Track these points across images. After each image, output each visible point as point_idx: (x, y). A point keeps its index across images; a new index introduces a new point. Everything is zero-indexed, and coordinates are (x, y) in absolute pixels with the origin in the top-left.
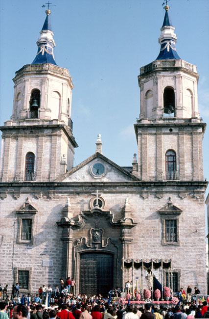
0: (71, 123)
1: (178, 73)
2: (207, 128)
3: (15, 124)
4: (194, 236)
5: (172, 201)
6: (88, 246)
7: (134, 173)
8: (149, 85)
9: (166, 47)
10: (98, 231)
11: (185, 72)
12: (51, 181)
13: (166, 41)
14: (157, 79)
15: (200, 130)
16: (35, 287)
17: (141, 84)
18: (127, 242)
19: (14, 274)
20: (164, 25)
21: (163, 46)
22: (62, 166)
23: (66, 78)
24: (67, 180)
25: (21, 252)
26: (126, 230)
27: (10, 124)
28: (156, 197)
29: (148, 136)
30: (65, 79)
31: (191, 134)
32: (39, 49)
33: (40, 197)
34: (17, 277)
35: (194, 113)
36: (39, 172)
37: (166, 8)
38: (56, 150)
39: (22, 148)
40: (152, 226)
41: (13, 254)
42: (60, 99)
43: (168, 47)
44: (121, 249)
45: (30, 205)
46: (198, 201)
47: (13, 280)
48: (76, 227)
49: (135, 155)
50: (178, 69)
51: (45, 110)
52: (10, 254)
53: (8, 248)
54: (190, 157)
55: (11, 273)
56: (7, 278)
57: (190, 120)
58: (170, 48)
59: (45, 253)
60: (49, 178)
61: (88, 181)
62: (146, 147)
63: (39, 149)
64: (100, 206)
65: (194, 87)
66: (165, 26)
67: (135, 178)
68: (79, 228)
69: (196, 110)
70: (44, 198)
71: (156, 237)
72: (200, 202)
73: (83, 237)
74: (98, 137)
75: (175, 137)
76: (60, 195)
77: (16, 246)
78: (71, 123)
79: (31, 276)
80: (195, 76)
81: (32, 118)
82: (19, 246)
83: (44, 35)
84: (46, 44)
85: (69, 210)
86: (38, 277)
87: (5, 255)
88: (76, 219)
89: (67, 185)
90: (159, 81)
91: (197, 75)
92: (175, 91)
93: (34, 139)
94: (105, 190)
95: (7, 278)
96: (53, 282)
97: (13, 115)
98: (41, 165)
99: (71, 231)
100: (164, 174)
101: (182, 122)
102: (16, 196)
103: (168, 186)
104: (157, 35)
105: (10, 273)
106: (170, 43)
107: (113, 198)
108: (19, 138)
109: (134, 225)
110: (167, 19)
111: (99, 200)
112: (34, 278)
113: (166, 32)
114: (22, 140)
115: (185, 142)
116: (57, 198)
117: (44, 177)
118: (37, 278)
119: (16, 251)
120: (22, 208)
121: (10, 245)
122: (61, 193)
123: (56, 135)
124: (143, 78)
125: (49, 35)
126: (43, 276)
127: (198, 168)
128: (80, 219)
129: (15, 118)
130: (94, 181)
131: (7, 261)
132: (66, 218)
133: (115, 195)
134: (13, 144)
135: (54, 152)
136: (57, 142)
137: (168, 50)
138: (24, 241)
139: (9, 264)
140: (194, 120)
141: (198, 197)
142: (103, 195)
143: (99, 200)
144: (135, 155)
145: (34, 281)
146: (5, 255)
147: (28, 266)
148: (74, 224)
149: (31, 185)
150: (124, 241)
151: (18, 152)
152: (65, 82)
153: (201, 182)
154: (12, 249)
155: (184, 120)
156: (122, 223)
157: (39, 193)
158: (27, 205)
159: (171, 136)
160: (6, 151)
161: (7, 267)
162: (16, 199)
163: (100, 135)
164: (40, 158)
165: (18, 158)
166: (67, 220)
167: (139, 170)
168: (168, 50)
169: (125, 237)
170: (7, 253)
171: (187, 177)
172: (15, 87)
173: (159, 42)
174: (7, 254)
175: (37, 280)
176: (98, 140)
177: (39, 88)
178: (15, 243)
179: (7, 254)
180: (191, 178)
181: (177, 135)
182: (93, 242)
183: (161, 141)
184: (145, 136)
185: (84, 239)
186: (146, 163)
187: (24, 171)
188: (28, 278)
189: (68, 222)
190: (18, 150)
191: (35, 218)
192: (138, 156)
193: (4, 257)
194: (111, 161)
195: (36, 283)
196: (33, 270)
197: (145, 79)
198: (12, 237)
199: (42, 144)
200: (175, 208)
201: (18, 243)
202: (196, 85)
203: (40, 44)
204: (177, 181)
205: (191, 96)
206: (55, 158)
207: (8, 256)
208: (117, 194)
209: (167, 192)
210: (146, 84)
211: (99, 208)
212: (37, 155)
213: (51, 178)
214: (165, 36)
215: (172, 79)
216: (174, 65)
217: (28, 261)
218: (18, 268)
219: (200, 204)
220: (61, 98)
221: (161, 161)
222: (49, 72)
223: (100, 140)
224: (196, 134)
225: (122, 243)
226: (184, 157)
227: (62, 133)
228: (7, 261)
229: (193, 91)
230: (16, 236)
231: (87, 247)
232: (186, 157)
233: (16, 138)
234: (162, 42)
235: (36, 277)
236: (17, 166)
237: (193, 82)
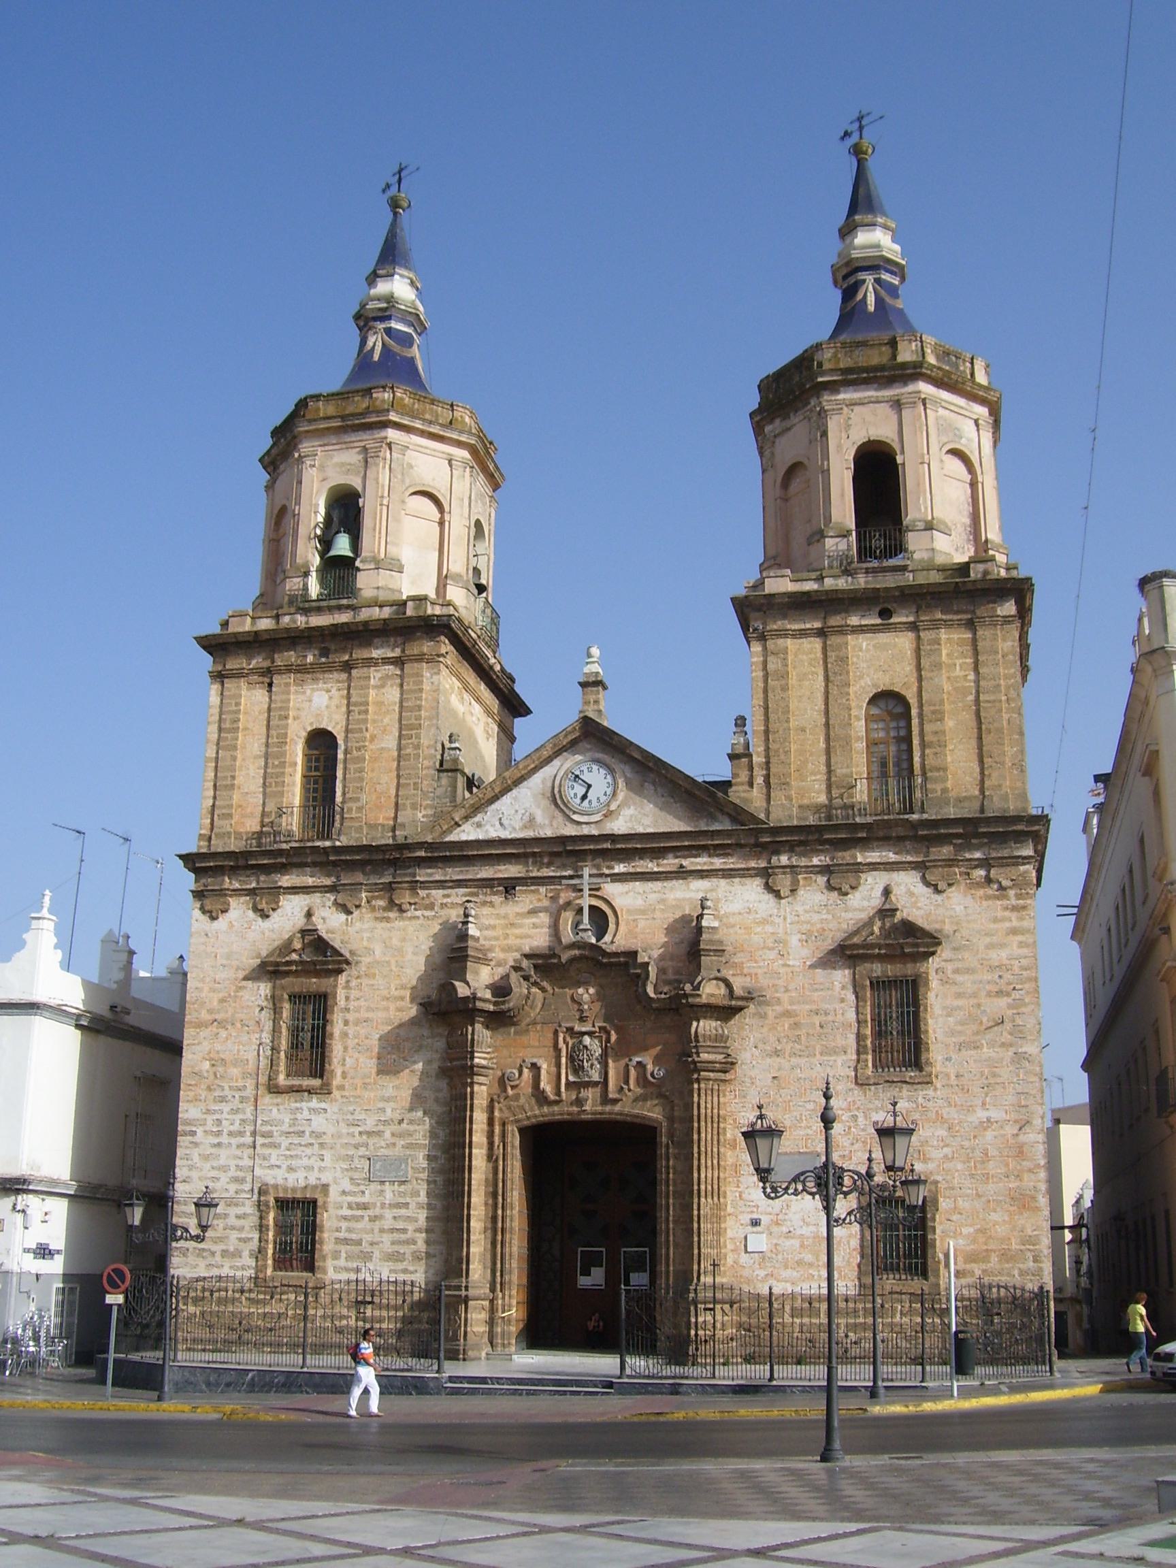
0: (394, 175)
1: (910, 388)
2: (1040, 603)
3: (265, 624)
4: (991, 1044)
5: (900, 898)
6: (552, 1097)
7: (737, 795)
8: (789, 448)
9: (860, 296)
10: (590, 1034)
11: (939, 383)
12: (400, 840)
13: (862, 276)
14: (822, 414)
15: (1009, 608)
16: (342, 1262)
17: (764, 444)
18: (712, 1075)
19: (261, 1207)
20: (854, 208)
21: (850, 293)
22: (445, 779)
23: (463, 438)
24: (468, 833)
25: (285, 1128)
26: (705, 1027)
27: (243, 623)
28: (830, 887)
29: (789, 642)
30: (459, 444)
31: (971, 625)
32: (364, 341)
33: (358, 907)
34: (271, 1222)
35: (982, 547)
36: (354, 806)
37: (857, 151)
38: (419, 718)
39: (286, 718)
40: (814, 1007)
41: (254, 1134)
42: (441, 523)
43: (869, 296)
44: (689, 1106)
45: (320, 938)
46: (1006, 897)
47: (256, 1236)
48: (500, 1019)
49: (741, 722)
50: (914, 372)
51: (378, 565)
52: (241, 1134)
53: (235, 1111)
54: (968, 717)
55: (249, 1208)
56: (233, 1228)
57: (964, 569)
58: (879, 301)
59: (381, 1128)
60: (394, 829)
61: (549, 833)
62: (785, 688)
63: (355, 716)
64: (601, 933)
65: (979, 442)
66: (857, 217)
67: (738, 814)
68: (514, 1024)
69: (992, 532)
70: (373, 909)
71: (834, 1051)
72: (1014, 901)
73: (529, 1061)
74: (589, 656)
75: (904, 642)
76: (437, 894)
77: (267, 1100)
78: (394, 175)
79: (328, 1220)
80: (983, 401)
81: (329, 597)
82: (279, 1099)
83: (382, 288)
84: (389, 318)
85: (470, 952)
86: (353, 1224)
87: (225, 1139)
88: (501, 990)
89: (465, 854)
90: (833, 424)
91: (992, 397)
92: (899, 459)
93: (336, 675)
94: (620, 868)
95: (233, 1228)
96: (414, 1242)
97: (262, 595)
98: (361, 779)
99: (481, 1033)
100: (861, 794)
101: (935, 577)
102: (263, 905)
103: (878, 839)
104: (829, 252)
105: (240, 1210)
106: (878, 281)
107: (653, 897)
108: (277, 679)
109: (740, 1003)
110: (861, 191)
111: (591, 907)
112: (338, 1230)
113: (862, 238)
114: (288, 685)
115: (944, 658)
116: (426, 909)
117: (372, 827)
118: (349, 1230)
119: (265, 1123)
120: (286, 947)
121: (243, 1100)
122: (441, 884)
123: (420, 658)
124: (772, 421)
125: (400, 287)
126: (373, 1219)
127: (1003, 763)
128: (519, 988)
129: (267, 602)
130: (570, 831)
131: (233, 1163)
132: (457, 984)
133: (657, 885)
134: (252, 698)
135: (411, 727)
136: (426, 687)
137: (871, 308)
138: (296, 1082)
139: (240, 1174)
140: (981, 567)
141: (1005, 883)
142: (612, 890)
143: (591, 907)
144: (741, 722)
145: (338, 1241)
146: (225, 1139)
147: (312, 1181)
148: (491, 1008)
149: (323, 859)
150: (698, 1071)
151: (273, 733)
152: (464, 454)
153: (1017, 819)
154: (249, 1114)
155: (942, 569)
156: (686, 996)
157: (355, 887)
158: (308, 939)
159: (883, 638)
160: (227, 728)
161: (233, 1187)
162: (265, 916)
163: (595, 651)
164: (359, 749)
165: (272, 754)
166: (462, 990)
167: (759, 780)
168: (871, 308)
169: (704, 1056)
170: (232, 1128)
171: (959, 800)
172: (270, 487)
173: (835, 283)
174: (231, 1134)
175: (347, 1235)
176: (587, 669)
177: (356, 483)
178: (262, 1090)
179: (231, 1134)
180: (976, 805)
181: (911, 635)
182: (571, 1078)
183: (844, 660)
184: (781, 641)
185: (535, 1068)
186: (787, 753)
187: (297, 801)
188: (311, 1229)
189: (466, 999)
190: (274, 719)
191: (341, 994)
192: (755, 725)
193: (219, 1145)
194: (638, 747)
195: (344, 1249)
196: (334, 1195)
197: (777, 421)
198: (251, 1067)
199: (367, 695)
200: (909, 929)
201: (274, 1089)
202: (987, 438)
203: (364, 320)
204: (915, 817)
205: (968, 478)
206: (417, 747)
207: (234, 1141)
208: (667, 884)
209: (874, 867)
210: (782, 442)
211: (593, 940)
212: (346, 739)
213: (403, 825)
214: (855, 254)
215: (891, 406)
216: (894, 357)
217: (312, 1162)
218: (276, 1187)
219: (1014, 908)
220: (447, 517)
221: (847, 742)
222: (393, 417)
223: (595, 668)
224: (994, 621)
225: (691, 1082)
226: (941, 720)
227: (446, 647)
228: (233, 1163)
229: (975, 459)
230: (264, 1062)
231: (546, 1098)
232: (950, 723)
233: (267, 676)
234: (845, 277)
235: (344, 1225)
236: (271, 781)
237: (976, 422)
